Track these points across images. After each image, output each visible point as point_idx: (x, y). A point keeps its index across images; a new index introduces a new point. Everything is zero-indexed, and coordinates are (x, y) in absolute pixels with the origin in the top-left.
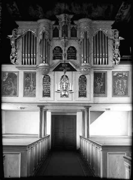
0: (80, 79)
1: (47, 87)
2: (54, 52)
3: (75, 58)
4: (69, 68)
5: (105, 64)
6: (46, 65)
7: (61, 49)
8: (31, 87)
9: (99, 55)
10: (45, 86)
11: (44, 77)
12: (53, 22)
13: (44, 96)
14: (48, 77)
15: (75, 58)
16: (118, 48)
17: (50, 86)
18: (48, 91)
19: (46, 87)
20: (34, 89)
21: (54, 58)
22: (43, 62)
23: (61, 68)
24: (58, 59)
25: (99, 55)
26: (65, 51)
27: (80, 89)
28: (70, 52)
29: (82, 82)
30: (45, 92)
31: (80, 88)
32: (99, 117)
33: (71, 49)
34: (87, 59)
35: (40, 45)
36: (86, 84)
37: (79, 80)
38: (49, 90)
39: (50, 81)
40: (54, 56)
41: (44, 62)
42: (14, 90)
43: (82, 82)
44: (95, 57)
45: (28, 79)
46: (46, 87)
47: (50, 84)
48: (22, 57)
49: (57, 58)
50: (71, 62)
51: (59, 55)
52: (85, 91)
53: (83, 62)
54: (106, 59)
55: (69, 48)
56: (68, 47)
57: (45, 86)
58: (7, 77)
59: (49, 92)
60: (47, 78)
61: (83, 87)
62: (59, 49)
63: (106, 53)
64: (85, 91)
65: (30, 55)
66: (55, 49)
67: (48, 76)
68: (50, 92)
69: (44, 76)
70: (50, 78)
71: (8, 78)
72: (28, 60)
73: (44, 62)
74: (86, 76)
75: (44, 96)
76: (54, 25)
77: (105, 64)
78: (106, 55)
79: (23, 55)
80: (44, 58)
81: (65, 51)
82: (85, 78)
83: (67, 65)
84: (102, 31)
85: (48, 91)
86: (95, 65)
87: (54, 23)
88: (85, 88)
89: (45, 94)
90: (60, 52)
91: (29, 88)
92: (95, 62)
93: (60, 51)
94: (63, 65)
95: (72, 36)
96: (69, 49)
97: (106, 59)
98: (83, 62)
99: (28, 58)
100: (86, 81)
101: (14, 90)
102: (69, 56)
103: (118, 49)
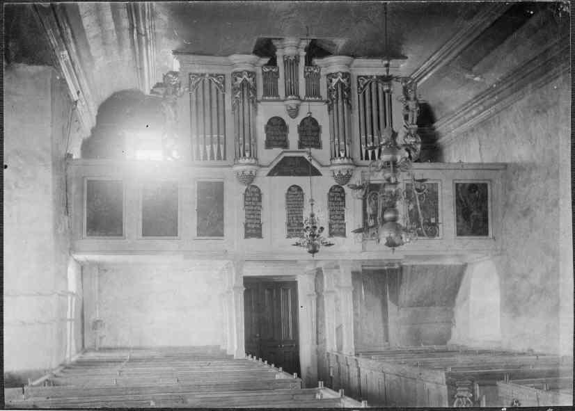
3: (318, 145)
7: (283, 122)
12: (265, 60)
13: (247, 236)
14: (255, 190)
15: (318, 145)
16: (415, 122)
22: (244, 155)
26: (293, 125)
27: (330, 218)
29: (336, 202)
30: (249, 225)
31: (330, 216)
34: (345, 148)
35: (331, 112)
37: (329, 197)
41: (247, 155)
43: (336, 202)
59: (258, 226)
67: (256, 187)
68: (261, 226)
70: (259, 190)
73: (247, 155)
74: (343, 187)
75: (247, 236)
76: (265, 65)
78: (222, 136)
80: (247, 144)
81: (293, 125)
86: (364, 162)
87: (267, 62)
89: (249, 231)
92: (222, 155)
95: (267, 93)
97: (222, 147)
99: (219, 143)
103: (417, 124)
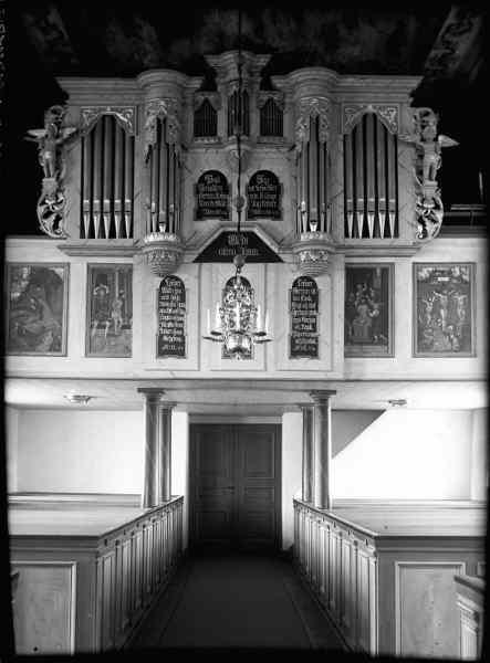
0: (296, 291)
1: (173, 321)
2: (197, 192)
4: (253, 252)
5: (387, 234)
7: (223, 179)
8: (116, 321)
9: (366, 203)
10: (168, 318)
11: (163, 284)
17: (182, 316)
18: (177, 336)
20: (125, 327)
21: (200, 215)
23: (224, 252)
24: (213, 216)
25: (366, 203)
27: (293, 329)
28: (258, 193)
30: (165, 338)
32: (366, 430)
33: (261, 179)
34: (319, 217)
36: (317, 309)
37: (292, 295)
38: (180, 332)
39: (183, 300)
40: (200, 208)
42: (50, 333)
44: (349, 208)
45: (105, 290)
46: (168, 322)
47: (184, 309)
48: (82, 211)
50: (260, 229)
51: (218, 203)
52: (313, 335)
53: (305, 229)
54: (392, 218)
55: (255, 175)
56: (251, 175)
57: (168, 318)
58: (27, 283)
59: (179, 339)
61: (306, 320)
62: (217, 181)
63: (390, 196)
64: (313, 335)
65: (112, 204)
69: (161, 279)
71: (28, 286)
72: (102, 220)
77: (385, 236)
79: (86, 202)
81: (239, 189)
82: (315, 285)
83: (246, 240)
84: (375, 116)
85: (177, 336)
88: (314, 325)
89: (166, 347)
90: (220, 192)
91: (108, 323)
93: (221, 188)
94: (232, 240)
95: (265, 132)
96: (253, 180)
98: (305, 229)
99: (102, 212)
100: (315, 298)
101: (50, 333)
102: (255, 208)
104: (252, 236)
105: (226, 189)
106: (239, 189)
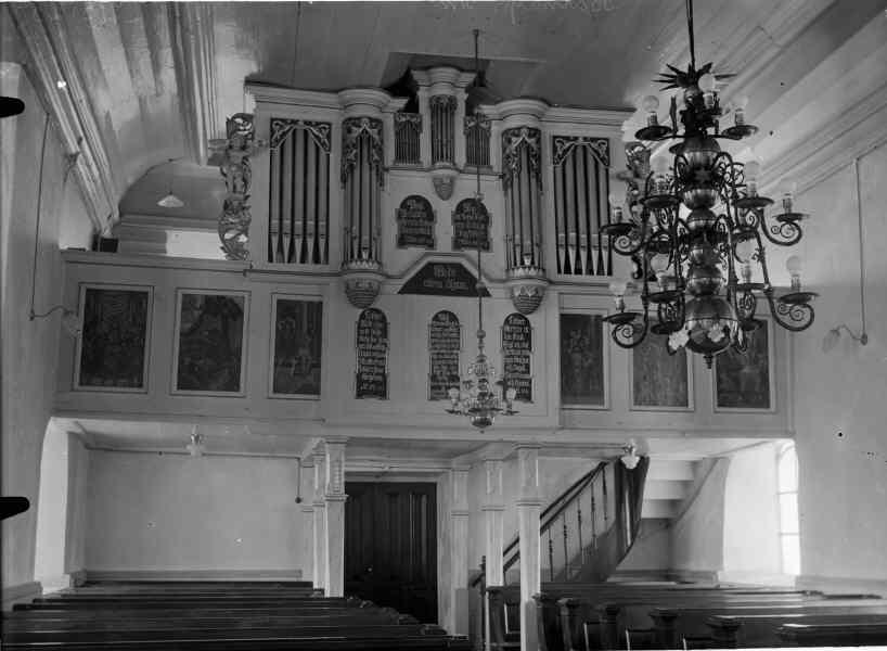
0: (508, 328)
1: (373, 358)
2: (399, 216)
4: (462, 286)
5: (600, 272)
6: (533, 272)
7: (427, 205)
8: (304, 358)
9: (566, 238)
10: (367, 354)
11: (362, 316)
12: (401, 103)
17: (384, 352)
18: (377, 374)
19: (367, 358)
20: (314, 366)
21: (402, 242)
23: (429, 283)
24: (416, 244)
25: (566, 238)
27: (505, 370)
28: (465, 221)
30: (365, 377)
32: (727, 488)
33: (467, 208)
34: (532, 250)
36: (530, 349)
37: (505, 333)
38: (381, 371)
39: (385, 333)
40: (402, 235)
42: (226, 371)
44: (296, 232)
45: (291, 324)
46: (367, 358)
47: (386, 345)
48: (557, 245)
49: (414, 240)
50: (468, 258)
51: (422, 231)
52: (526, 376)
53: (356, 256)
54: (322, 242)
55: (462, 203)
56: (458, 201)
57: (367, 354)
58: (200, 312)
59: (380, 378)
60: (373, 321)
61: (517, 360)
62: (421, 207)
63: (570, 230)
64: (526, 376)
65: (578, 238)
66: (404, 205)
69: (361, 311)
71: (201, 316)
72: (578, 257)
77: (598, 273)
79: (562, 235)
81: (444, 210)
82: (527, 323)
83: (454, 272)
84: (584, 147)
85: (377, 374)
88: (528, 366)
89: (365, 386)
90: (424, 219)
91: (294, 362)
93: (425, 215)
94: (438, 272)
95: (400, 156)
96: (460, 208)
98: (356, 256)
99: (292, 235)
100: (528, 337)
101: (226, 371)
102: (462, 238)
104: (459, 267)
105: (430, 215)
106: (444, 210)
